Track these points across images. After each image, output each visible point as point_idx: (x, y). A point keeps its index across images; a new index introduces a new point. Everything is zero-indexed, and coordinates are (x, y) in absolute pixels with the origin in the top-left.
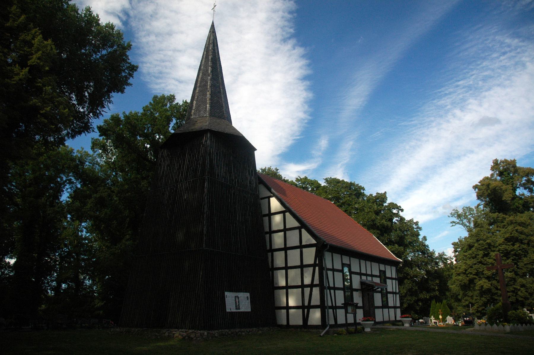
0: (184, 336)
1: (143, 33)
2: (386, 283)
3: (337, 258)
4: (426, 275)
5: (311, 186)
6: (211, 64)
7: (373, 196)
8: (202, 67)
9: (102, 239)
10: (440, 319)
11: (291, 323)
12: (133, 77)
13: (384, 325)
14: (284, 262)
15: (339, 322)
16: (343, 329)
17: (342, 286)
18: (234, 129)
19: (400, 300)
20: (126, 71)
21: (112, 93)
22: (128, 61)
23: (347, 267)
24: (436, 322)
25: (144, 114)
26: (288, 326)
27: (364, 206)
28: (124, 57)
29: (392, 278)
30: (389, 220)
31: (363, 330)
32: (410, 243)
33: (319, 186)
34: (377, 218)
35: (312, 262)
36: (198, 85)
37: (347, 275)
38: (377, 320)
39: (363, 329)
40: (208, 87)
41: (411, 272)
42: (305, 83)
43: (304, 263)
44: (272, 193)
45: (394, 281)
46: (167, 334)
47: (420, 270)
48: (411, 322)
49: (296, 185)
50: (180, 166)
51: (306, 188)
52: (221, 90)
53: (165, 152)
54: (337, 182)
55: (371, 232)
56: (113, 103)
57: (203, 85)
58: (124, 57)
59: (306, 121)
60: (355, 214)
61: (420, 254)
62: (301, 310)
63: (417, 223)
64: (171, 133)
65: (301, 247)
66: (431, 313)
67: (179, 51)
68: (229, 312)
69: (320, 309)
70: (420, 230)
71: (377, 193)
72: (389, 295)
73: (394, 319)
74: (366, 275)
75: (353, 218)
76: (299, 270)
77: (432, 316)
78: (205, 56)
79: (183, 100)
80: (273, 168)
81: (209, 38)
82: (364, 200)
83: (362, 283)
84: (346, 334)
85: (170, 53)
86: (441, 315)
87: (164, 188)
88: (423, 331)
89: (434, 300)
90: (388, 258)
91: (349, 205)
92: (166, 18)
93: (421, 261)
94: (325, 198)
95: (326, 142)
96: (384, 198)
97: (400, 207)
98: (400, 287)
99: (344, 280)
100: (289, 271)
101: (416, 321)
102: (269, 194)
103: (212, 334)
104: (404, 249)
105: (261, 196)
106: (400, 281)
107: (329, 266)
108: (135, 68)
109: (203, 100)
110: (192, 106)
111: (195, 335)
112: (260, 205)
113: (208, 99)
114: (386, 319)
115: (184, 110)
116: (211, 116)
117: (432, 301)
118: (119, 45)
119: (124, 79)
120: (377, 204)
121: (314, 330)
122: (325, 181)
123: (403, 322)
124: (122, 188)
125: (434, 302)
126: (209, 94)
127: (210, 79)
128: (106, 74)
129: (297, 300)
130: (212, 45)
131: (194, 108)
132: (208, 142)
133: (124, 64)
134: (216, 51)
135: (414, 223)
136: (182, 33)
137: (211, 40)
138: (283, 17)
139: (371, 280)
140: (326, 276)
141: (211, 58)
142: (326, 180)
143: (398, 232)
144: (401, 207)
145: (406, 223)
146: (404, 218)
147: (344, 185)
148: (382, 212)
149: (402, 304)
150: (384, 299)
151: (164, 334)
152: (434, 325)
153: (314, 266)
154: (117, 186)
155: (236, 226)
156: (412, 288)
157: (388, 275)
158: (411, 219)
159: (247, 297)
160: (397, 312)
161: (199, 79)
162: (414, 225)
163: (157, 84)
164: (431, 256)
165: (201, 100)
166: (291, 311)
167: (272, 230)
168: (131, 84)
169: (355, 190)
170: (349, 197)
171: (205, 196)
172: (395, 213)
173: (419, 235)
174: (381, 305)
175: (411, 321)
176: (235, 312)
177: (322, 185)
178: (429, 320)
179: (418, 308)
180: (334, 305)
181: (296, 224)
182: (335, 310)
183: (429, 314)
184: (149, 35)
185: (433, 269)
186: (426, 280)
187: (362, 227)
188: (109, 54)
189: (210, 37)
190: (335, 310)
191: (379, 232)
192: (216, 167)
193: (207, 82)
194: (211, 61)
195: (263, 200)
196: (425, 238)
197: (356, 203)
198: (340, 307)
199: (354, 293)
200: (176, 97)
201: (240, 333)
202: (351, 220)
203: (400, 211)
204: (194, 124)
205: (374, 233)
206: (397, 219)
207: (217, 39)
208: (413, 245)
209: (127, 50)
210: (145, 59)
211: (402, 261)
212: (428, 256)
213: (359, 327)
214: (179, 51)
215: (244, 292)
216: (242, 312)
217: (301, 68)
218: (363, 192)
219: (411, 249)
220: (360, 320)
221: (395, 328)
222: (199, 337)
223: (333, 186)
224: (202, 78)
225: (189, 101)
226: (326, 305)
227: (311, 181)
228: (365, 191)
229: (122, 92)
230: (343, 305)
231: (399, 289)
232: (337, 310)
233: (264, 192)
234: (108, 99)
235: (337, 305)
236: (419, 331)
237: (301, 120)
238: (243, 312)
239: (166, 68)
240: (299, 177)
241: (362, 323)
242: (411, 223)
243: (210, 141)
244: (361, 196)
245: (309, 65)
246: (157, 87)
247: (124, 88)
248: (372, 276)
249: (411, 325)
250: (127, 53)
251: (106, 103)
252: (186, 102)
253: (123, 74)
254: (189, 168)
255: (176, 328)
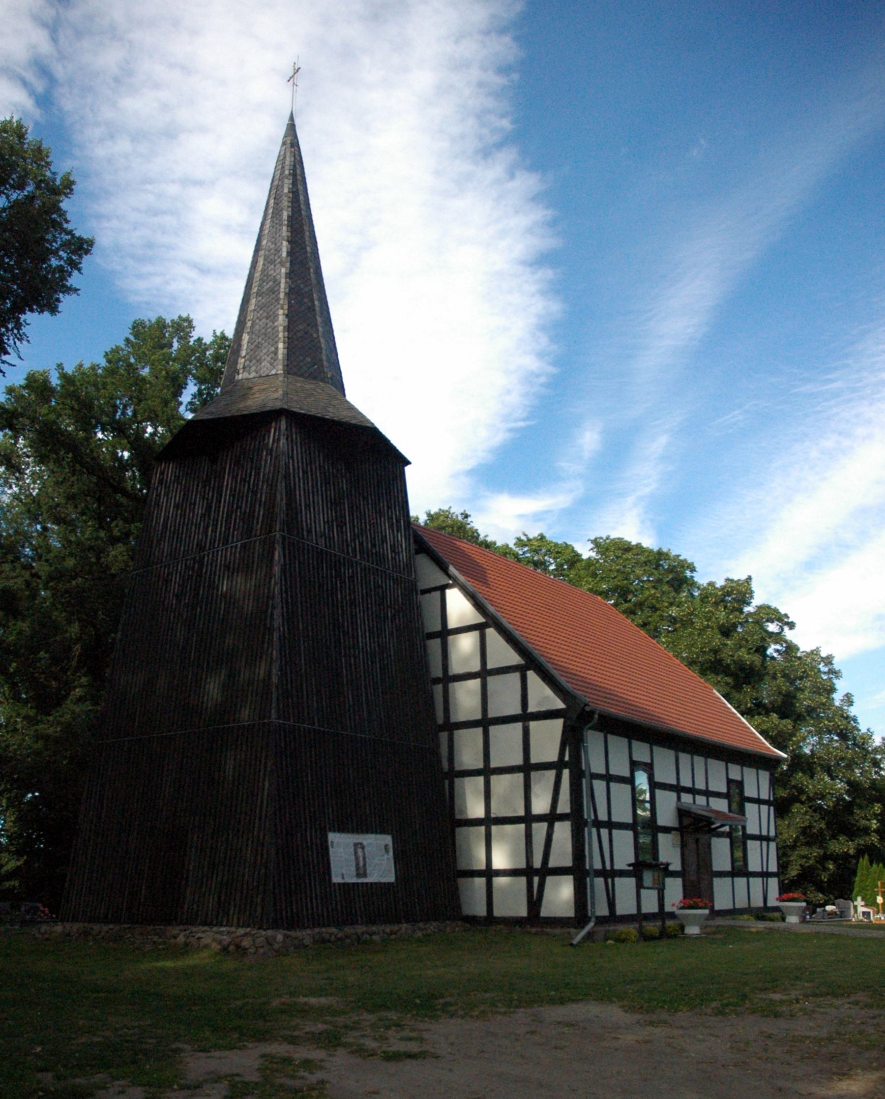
0: (225, 943)
1: (97, 133)
2: (742, 811)
3: (618, 745)
4: (848, 792)
5: (555, 558)
6: (289, 234)
7: (718, 585)
8: (264, 242)
9: (12, 699)
10: (878, 905)
11: (497, 913)
12: (79, 270)
13: (734, 919)
14: (481, 756)
15: (620, 910)
16: (631, 929)
17: (629, 820)
18: (352, 408)
19: (779, 858)
20: (61, 253)
21: (25, 313)
22: (65, 226)
23: (645, 771)
24: (869, 913)
25: (111, 372)
26: (490, 919)
27: (692, 614)
28: (54, 216)
29: (758, 801)
30: (757, 651)
31: (680, 932)
32: (811, 711)
33: (575, 559)
34: (726, 645)
35: (552, 756)
36: (255, 290)
37: (643, 792)
38: (717, 907)
39: (682, 928)
40: (282, 296)
41: (811, 786)
42: (540, 274)
43: (534, 760)
44: (450, 577)
45: (764, 808)
46: (181, 939)
47: (832, 779)
48: (804, 912)
49: (516, 556)
50: (209, 507)
51: (540, 565)
52: (316, 303)
53: (171, 470)
54: (624, 548)
55: (707, 680)
56: (28, 341)
57: (267, 289)
58: (54, 216)
59: (543, 380)
60: (670, 634)
61: (836, 738)
62: (523, 880)
63: (828, 660)
64: (184, 420)
65: (525, 717)
66: (856, 889)
67: (199, 183)
68: (339, 884)
69: (571, 878)
70: (837, 677)
71: (727, 580)
72: (750, 843)
73: (761, 905)
74: (692, 791)
75: (664, 643)
76: (520, 776)
77: (859, 898)
78: (270, 211)
79: (214, 331)
80: (457, 510)
81: (281, 161)
82: (692, 596)
83: (682, 813)
84: (638, 941)
85: (173, 189)
86: (882, 896)
87: (169, 565)
88: (833, 934)
89: (866, 857)
90: (749, 748)
91: (654, 609)
92: (157, 86)
93: (836, 756)
94: (590, 590)
95: (596, 436)
96: (745, 593)
97: (786, 616)
98: (779, 822)
99: (635, 802)
100: (494, 779)
101: (818, 910)
102: (444, 580)
103: (296, 938)
104: (794, 727)
105: (423, 585)
106: (781, 808)
107: (597, 767)
108: (85, 246)
109: (269, 330)
110: (240, 346)
111: (252, 942)
112: (419, 607)
113: (281, 328)
114: (741, 903)
115: (217, 358)
116: (289, 374)
117: (861, 860)
118: (41, 181)
119: (57, 276)
120: (725, 607)
121: (558, 931)
122: (592, 546)
123: (784, 910)
124: (59, 566)
125: (864, 861)
126: (284, 314)
127: (286, 273)
128: (8, 263)
129: (514, 854)
130: (291, 181)
131: (243, 353)
132: (283, 441)
133: (54, 236)
134: (302, 197)
135: (822, 658)
136: (203, 130)
137: (287, 168)
138: (481, 84)
139: (705, 803)
140: (589, 793)
141: (288, 216)
142: (596, 543)
143: (780, 681)
144: (788, 617)
145: (800, 658)
146: (796, 645)
147: (643, 558)
148: (740, 630)
149: (783, 866)
150: (739, 854)
151: (175, 937)
152: (861, 921)
153: (558, 766)
154: (47, 561)
155: (355, 662)
156: (810, 827)
157: (750, 791)
158: (814, 648)
159: (386, 846)
160: (769, 885)
161: (257, 275)
162: (822, 664)
163: (140, 276)
164: (863, 744)
165: (263, 331)
166: (500, 882)
167: (451, 673)
168: (76, 290)
169: (671, 570)
170: (654, 587)
171: (276, 584)
172: (772, 633)
173: (832, 690)
174: (728, 867)
175: (806, 908)
176: (353, 884)
177: (585, 557)
178: (849, 908)
179: (824, 877)
180: (608, 867)
181: (514, 658)
182: (610, 880)
183: (851, 892)
184: (112, 137)
185: (868, 778)
186: (849, 807)
187: (687, 669)
188: (11, 207)
189: (285, 158)
190: (610, 880)
191: (729, 680)
192: (303, 508)
193: (277, 283)
194: (288, 226)
195: (427, 596)
196: (849, 699)
197: (671, 604)
198: (622, 873)
199: (661, 837)
200: (194, 323)
201: (368, 937)
202: (660, 648)
203: (786, 628)
204: (244, 397)
205: (717, 684)
206: (778, 647)
207: (302, 163)
208: (818, 715)
209: (62, 198)
210: (105, 208)
211: (785, 756)
212: (854, 744)
213: (669, 923)
214: (199, 183)
215: (376, 833)
216: (371, 883)
217: (530, 231)
218: (692, 577)
219: (813, 725)
220: (673, 905)
221: (762, 926)
222: (262, 947)
223: (612, 560)
224: (263, 271)
225: (230, 333)
226: (588, 867)
227: (556, 545)
228: (695, 574)
229: (54, 310)
230: (631, 868)
231: (776, 828)
232: (616, 879)
233: (429, 575)
234: (15, 331)
235: (616, 867)
236: (824, 934)
237: (529, 377)
238: (376, 883)
239: (164, 233)
240: (525, 535)
241: (678, 912)
242: (813, 659)
243: (287, 439)
244: (685, 586)
245: (552, 224)
246: (141, 285)
247: (58, 300)
248: (708, 793)
249: (803, 920)
250: (61, 204)
251: (11, 342)
252: (223, 337)
253: (54, 262)
254: (232, 512)
255: (204, 923)
